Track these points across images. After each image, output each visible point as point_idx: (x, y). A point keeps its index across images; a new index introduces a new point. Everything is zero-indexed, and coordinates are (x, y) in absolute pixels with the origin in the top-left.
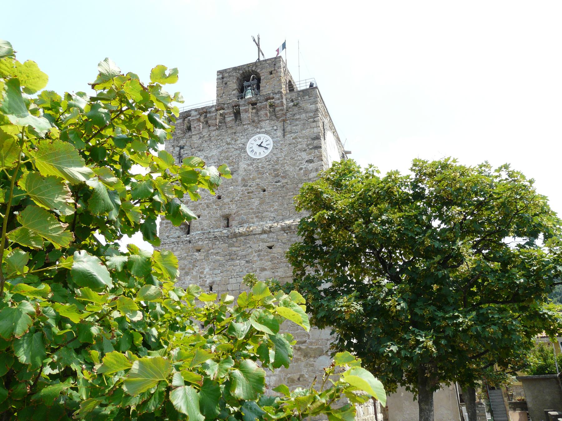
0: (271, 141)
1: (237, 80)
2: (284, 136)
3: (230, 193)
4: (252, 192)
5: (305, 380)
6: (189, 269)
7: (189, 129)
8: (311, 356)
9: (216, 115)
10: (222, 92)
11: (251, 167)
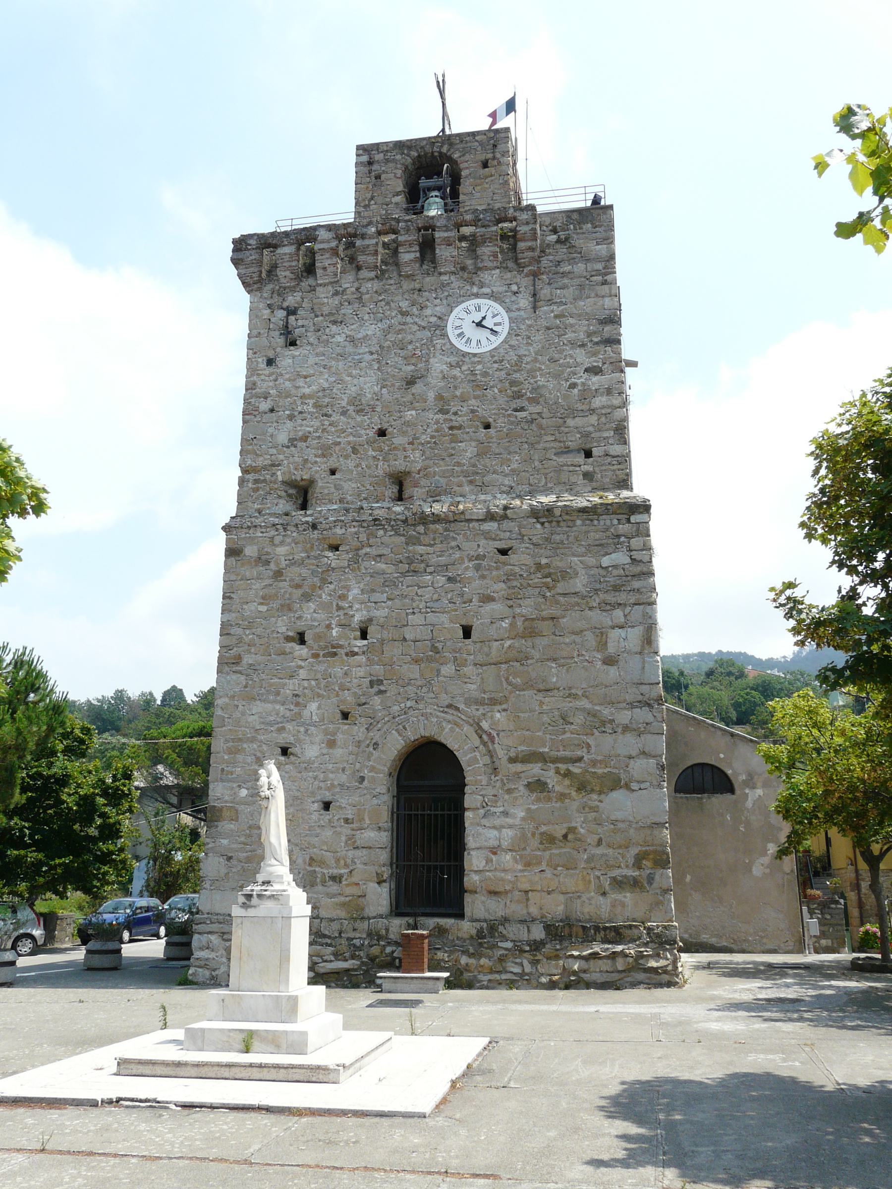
0: (504, 317)
1: (404, 172)
2: (535, 308)
3: (407, 424)
4: (460, 428)
5: (580, 840)
6: (313, 587)
7: (310, 270)
8: (592, 790)
9: (377, 244)
10: (369, 196)
11: (456, 372)
